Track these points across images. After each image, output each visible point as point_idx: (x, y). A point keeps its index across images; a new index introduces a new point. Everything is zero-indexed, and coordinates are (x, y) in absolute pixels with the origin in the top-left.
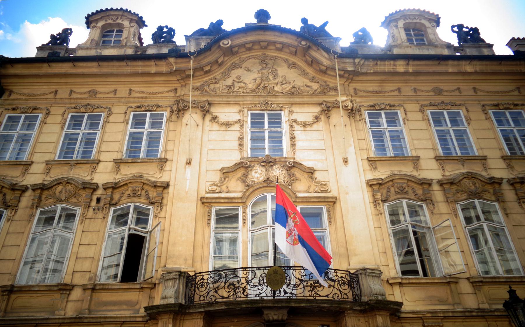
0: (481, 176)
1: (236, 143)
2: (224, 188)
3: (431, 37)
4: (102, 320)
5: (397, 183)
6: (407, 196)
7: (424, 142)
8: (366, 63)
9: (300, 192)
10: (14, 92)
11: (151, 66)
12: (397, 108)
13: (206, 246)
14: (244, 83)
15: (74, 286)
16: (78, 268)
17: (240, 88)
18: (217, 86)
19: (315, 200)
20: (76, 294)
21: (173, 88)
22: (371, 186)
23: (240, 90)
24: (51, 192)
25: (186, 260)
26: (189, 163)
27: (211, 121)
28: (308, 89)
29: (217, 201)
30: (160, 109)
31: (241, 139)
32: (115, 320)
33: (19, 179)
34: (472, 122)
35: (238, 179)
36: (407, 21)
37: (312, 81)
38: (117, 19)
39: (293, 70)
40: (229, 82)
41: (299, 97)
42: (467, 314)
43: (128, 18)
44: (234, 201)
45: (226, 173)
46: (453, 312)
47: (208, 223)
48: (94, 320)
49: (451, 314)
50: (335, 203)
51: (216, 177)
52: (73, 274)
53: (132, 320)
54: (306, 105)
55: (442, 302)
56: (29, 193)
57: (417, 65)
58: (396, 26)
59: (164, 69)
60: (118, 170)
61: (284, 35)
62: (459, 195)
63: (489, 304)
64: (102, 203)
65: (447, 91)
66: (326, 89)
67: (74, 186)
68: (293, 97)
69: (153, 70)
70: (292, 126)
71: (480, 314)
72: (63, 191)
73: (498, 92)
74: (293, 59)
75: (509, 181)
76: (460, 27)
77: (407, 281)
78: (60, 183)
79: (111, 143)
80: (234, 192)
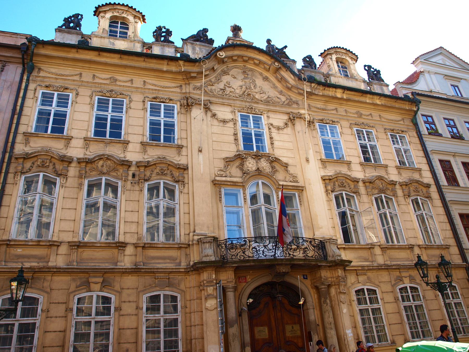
0: (386, 179)
1: (232, 138)
2: (228, 172)
3: (353, 71)
4: (155, 270)
5: (40, 158)
6: (345, 189)
7: (353, 151)
8: (318, 87)
9: (280, 180)
10: (43, 70)
11: (163, 64)
12: (336, 124)
13: (220, 217)
14: (233, 88)
15: (61, 243)
16: (128, 230)
17: (230, 92)
18: (213, 88)
19: (291, 188)
20: (129, 250)
21: (179, 85)
22: (324, 180)
23: (231, 94)
24: (94, 166)
25: (208, 227)
26: (200, 151)
27: (212, 117)
28: (279, 100)
29: (225, 183)
30: (171, 102)
31: (235, 135)
32: (165, 270)
33: (62, 151)
34: (379, 140)
35: (237, 167)
36: (338, 56)
37: (281, 94)
38: (123, 13)
39: (266, 83)
40: (221, 86)
41: (273, 106)
42: (380, 268)
43: (133, 14)
44: (237, 184)
45: (228, 161)
46: (373, 266)
47: (220, 200)
48: (149, 271)
49: (371, 268)
50: (303, 190)
51: (221, 164)
52: (124, 234)
53: (177, 270)
54: (278, 113)
55: (366, 260)
56: (73, 165)
57: (349, 94)
58: (331, 59)
59: (174, 69)
60: (145, 151)
61: (249, 50)
62: (373, 190)
63: (390, 261)
64: (137, 178)
65: (365, 115)
66: (291, 102)
67: (113, 162)
68: (269, 105)
69: (165, 68)
70: (270, 129)
71: (386, 267)
72: (105, 166)
73: (392, 120)
74: (266, 74)
75: (363, 181)
76: (370, 67)
77: (348, 247)
78: (102, 159)
79: (136, 127)
80: (235, 177)
